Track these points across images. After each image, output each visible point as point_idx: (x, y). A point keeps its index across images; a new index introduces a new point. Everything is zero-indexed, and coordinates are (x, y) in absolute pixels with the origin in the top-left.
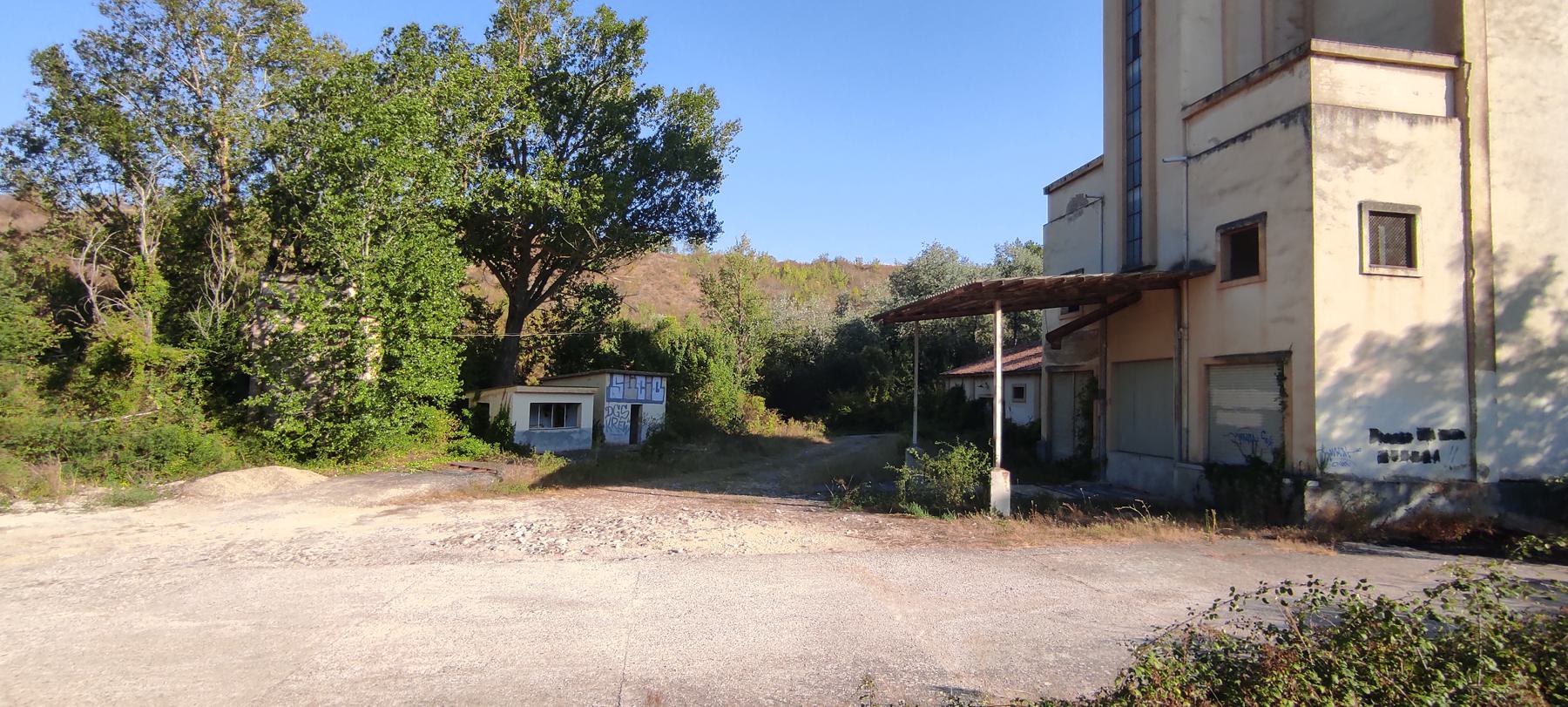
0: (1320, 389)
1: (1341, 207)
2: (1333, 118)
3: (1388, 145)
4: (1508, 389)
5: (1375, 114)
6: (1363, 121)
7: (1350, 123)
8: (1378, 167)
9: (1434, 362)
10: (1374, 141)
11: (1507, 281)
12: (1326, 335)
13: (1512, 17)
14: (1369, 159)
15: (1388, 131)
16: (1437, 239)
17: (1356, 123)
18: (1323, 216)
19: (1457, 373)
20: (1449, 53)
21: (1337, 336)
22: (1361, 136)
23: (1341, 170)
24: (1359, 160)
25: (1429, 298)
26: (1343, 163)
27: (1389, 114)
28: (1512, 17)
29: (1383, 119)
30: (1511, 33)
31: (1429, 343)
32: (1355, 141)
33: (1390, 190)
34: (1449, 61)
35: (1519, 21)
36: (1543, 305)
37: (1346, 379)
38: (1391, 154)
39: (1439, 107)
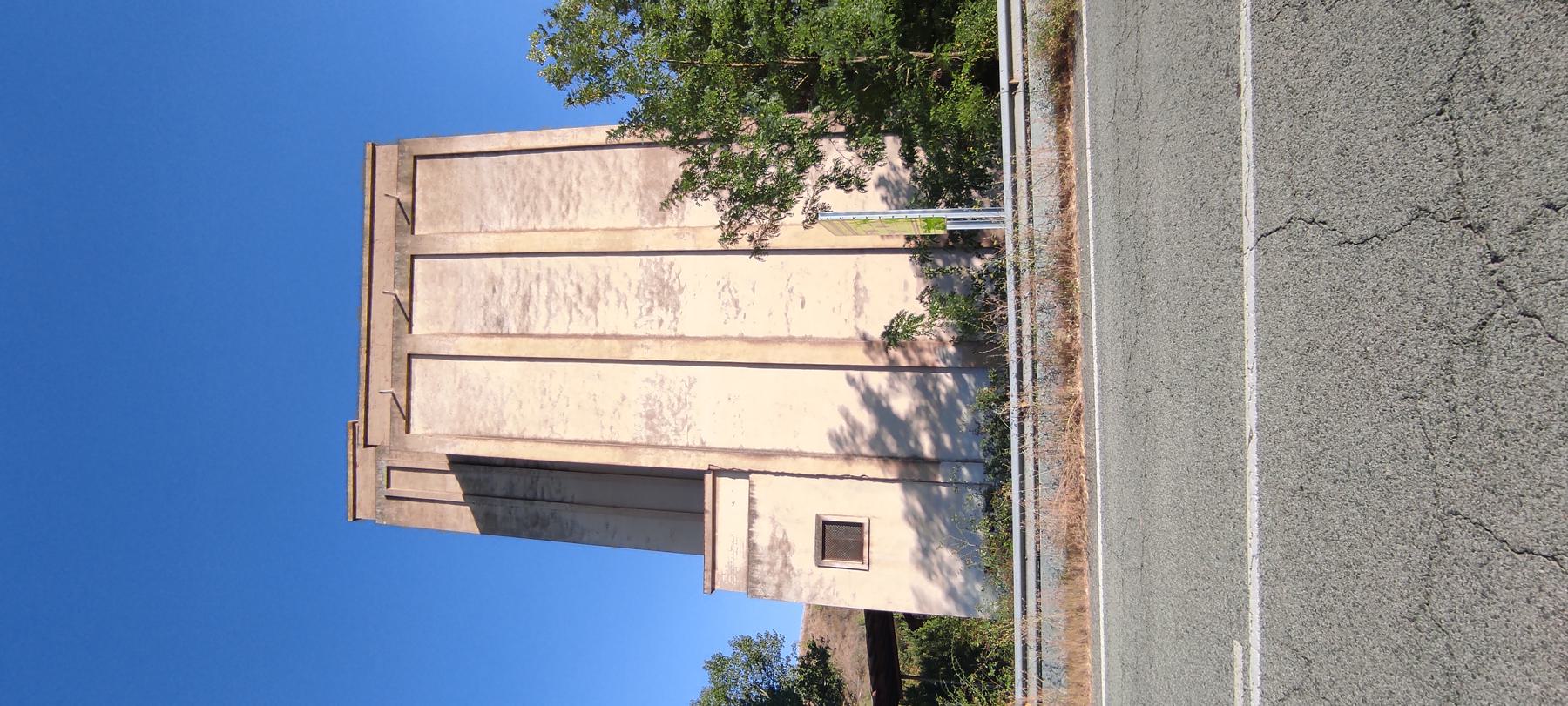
0: (957, 613)
1: (821, 581)
2: (757, 582)
3: (773, 536)
4: (953, 441)
5: (751, 546)
6: (758, 557)
7: (759, 567)
8: (789, 548)
9: (933, 505)
10: (771, 548)
11: (866, 420)
12: (920, 607)
13: (671, 420)
14: (784, 553)
15: (762, 540)
16: (844, 503)
17: (759, 562)
18: (828, 598)
19: (916, 363)
20: (702, 479)
21: (919, 597)
22: (767, 559)
23: (794, 580)
24: (786, 564)
25: (884, 507)
26: (788, 576)
27: (750, 534)
28: (671, 420)
29: (756, 539)
30: (684, 421)
31: (918, 507)
32: (772, 564)
33: (805, 541)
34: (708, 478)
35: (674, 414)
36: (887, 398)
37: (951, 593)
38: (780, 536)
39: (742, 483)
